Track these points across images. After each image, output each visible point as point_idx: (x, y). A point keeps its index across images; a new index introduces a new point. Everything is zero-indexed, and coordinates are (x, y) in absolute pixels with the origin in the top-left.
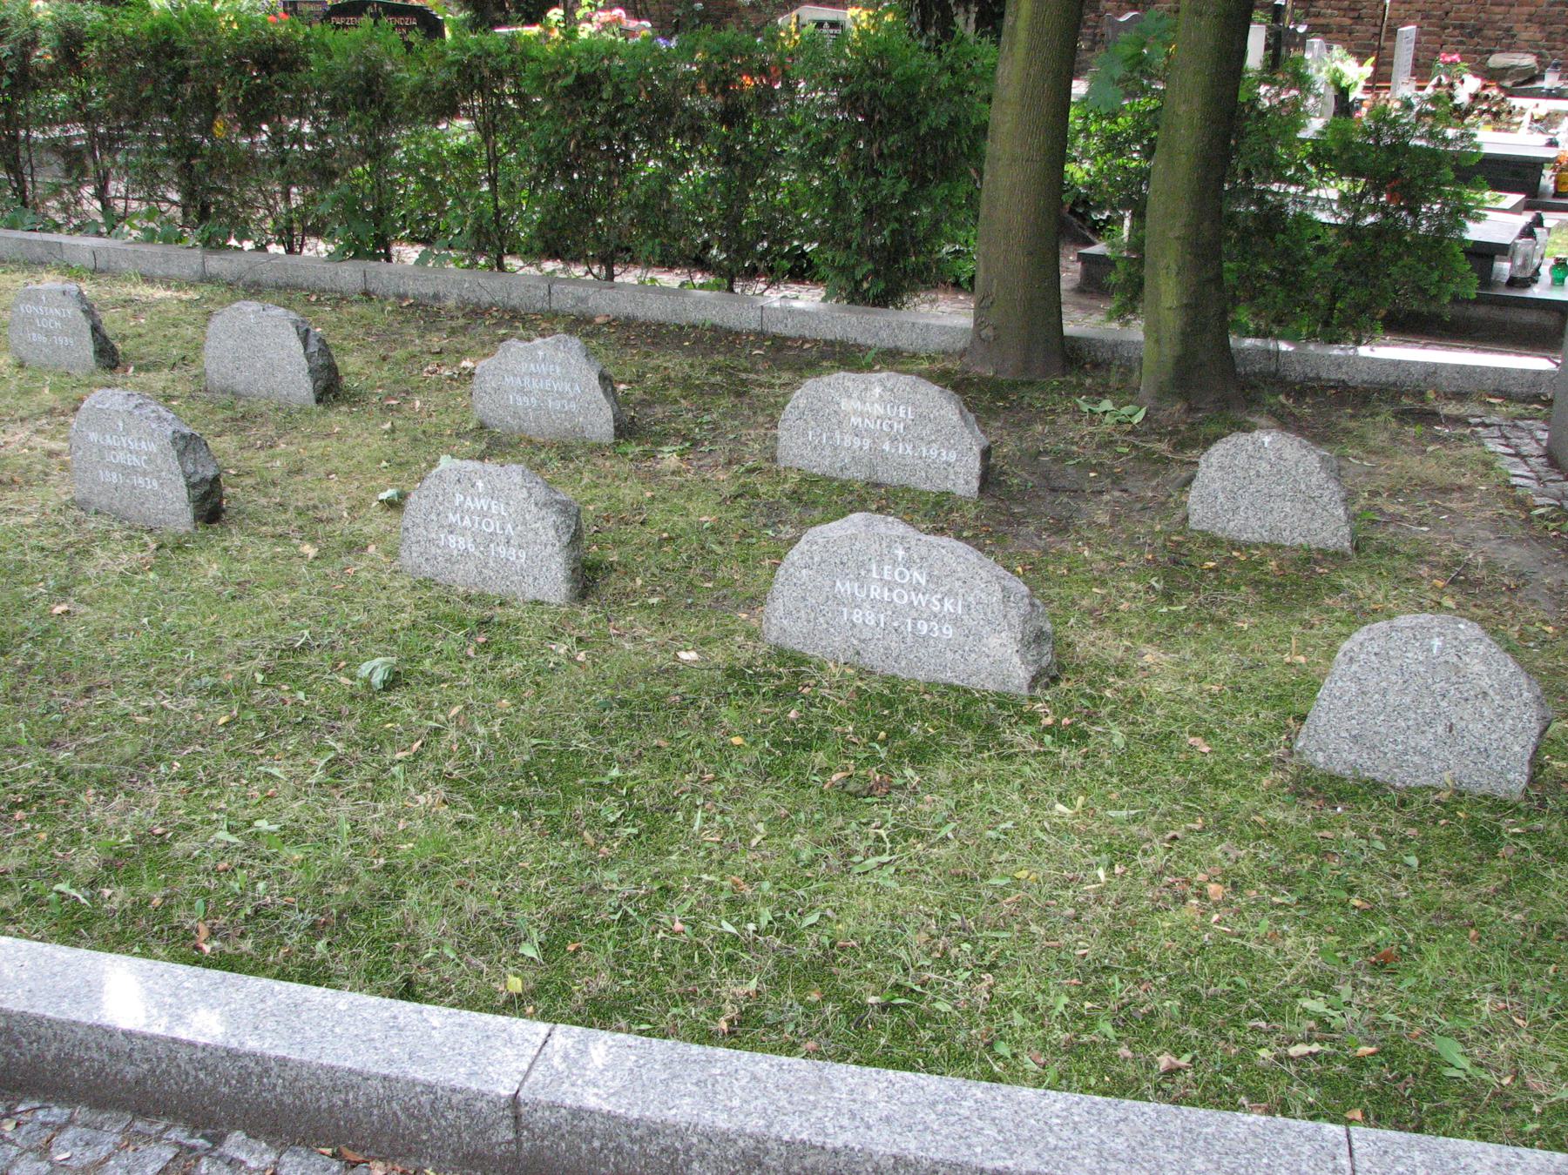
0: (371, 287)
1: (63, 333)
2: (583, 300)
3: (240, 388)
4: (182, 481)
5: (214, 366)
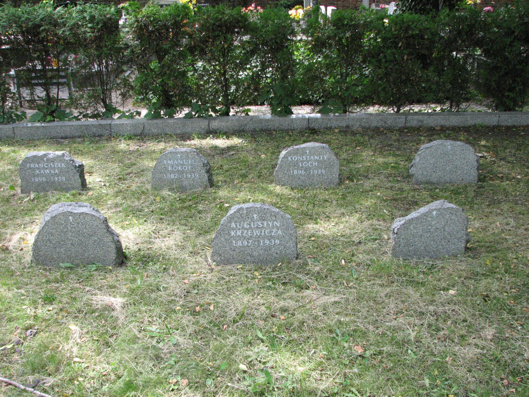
1: (317, 168)
2: (421, 121)
3: (435, 180)
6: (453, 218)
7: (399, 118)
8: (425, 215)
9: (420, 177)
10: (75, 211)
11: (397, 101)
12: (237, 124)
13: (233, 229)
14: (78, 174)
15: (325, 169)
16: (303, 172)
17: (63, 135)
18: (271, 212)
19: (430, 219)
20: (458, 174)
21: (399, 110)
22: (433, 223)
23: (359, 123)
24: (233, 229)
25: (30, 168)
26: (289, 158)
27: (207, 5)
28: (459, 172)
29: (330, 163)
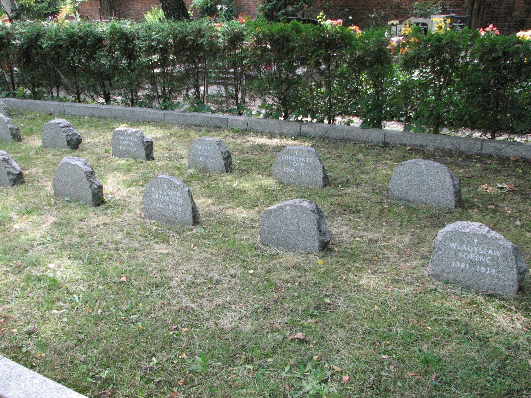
0: (388, 141)
1: (305, 169)
2: (500, 150)
3: (410, 198)
4: (515, 271)
5: (395, 187)
6: (304, 216)
7: (475, 143)
8: (281, 208)
9: (395, 192)
10: (73, 163)
11: (494, 127)
12: (323, 131)
13: (153, 193)
14: (144, 148)
15: (311, 170)
16: (294, 171)
17: (195, 123)
18: (175, 184)
19: (285, 213)
20: (434, 196)
21: (493, 137)
22: (289, 217)
23: (433, 144)
24: (153, 193)
25: (117, 139)
26: (282, 157)
27: (462, 24)
28: (435, 194)
29: (315, 166)
